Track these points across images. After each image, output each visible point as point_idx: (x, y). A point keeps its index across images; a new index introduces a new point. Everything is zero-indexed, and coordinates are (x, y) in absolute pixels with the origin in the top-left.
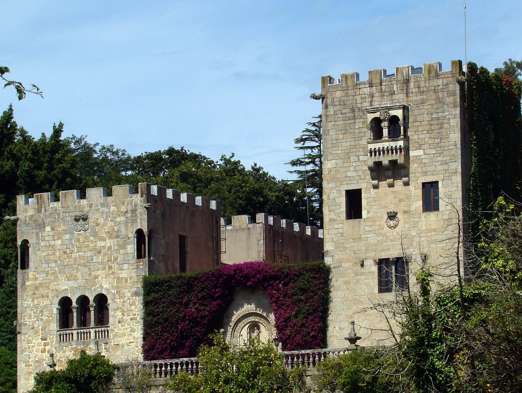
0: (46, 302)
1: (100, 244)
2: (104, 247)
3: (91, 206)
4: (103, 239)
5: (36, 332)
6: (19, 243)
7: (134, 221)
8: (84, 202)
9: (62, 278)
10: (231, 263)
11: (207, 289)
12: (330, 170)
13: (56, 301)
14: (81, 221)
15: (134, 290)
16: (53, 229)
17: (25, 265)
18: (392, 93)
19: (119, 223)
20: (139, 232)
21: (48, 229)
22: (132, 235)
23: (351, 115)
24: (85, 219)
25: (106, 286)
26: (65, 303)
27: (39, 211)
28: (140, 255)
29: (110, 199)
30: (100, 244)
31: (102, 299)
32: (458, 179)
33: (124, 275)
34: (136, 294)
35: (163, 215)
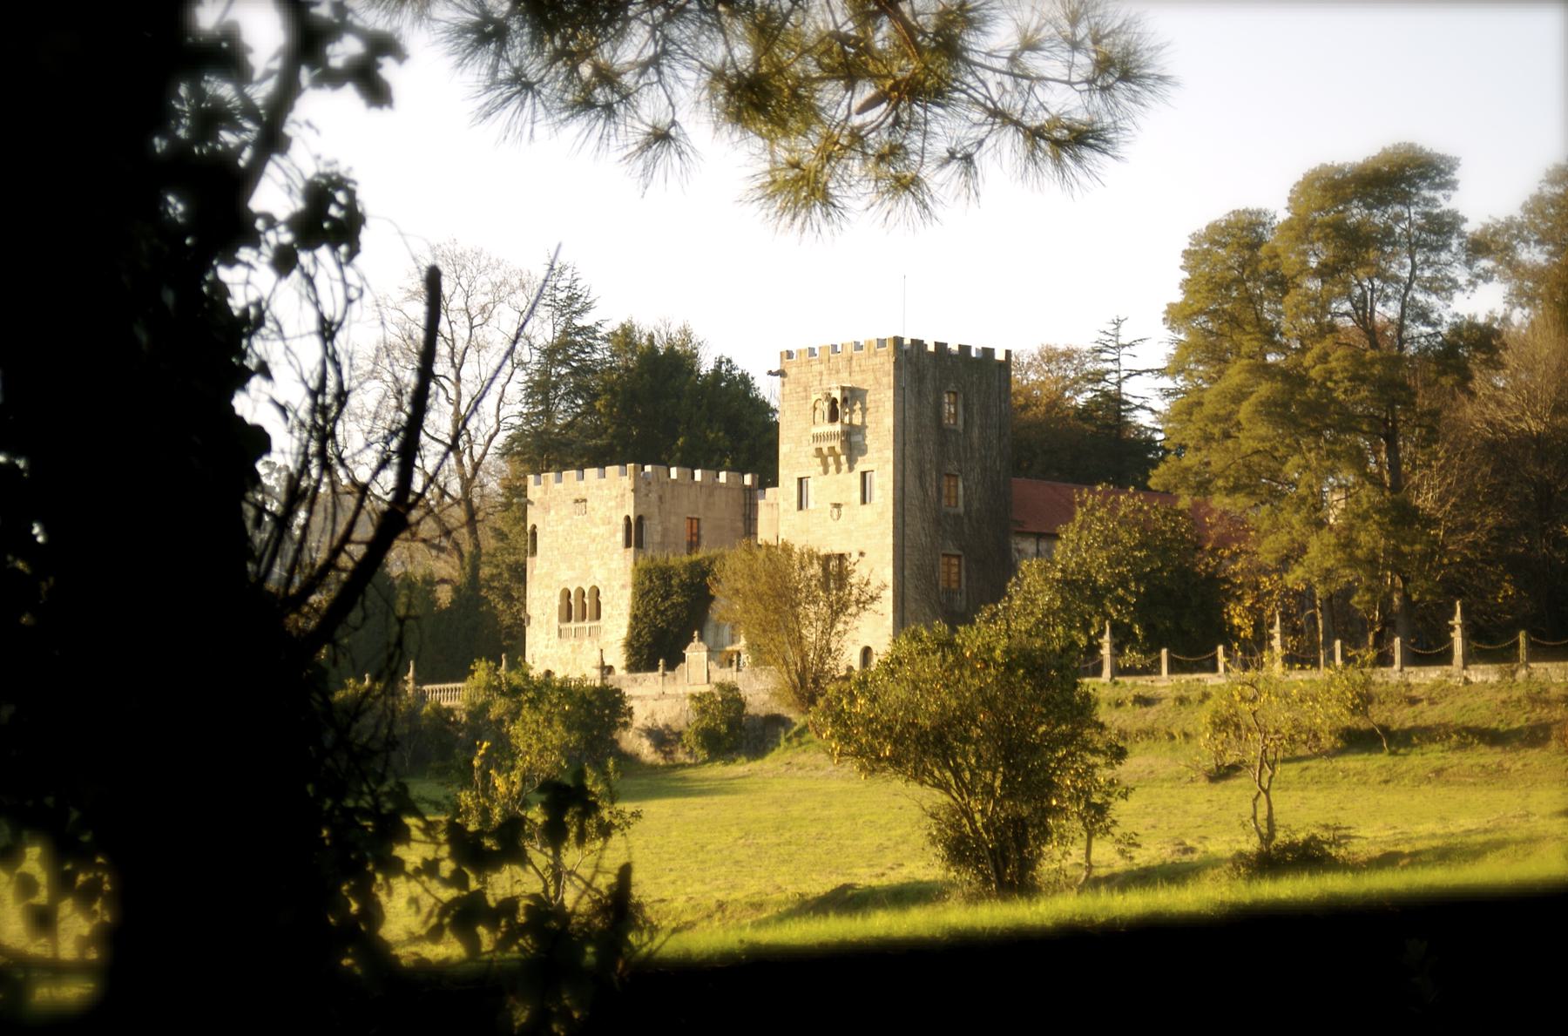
0: (550, 593)
1: (595, 531)
2: (597, 535)
3: (587, 488)
4: (596, 525)
5: (541, 627)
6: (529, 527)
7: (623, 507)
8: (582, 483)
9: (563, 566)
10: (238, 411)
11: (1014, 778)
12: (785, 455)
13: (558, 592)
14: (1196, 410)
15: (621, 582)
16: (557, 513)
17: (534, 552)
18: (838, 372)
19: (611, 508)
20: (628, 518)
21: (552, 512)
22: (621, 522)
23: (803, 394)
24: (585, 500)
25: (598, 577)
26: (567, 594)
27: (546, 493)
28: (628, 545)
29: (603, 480)
30: (595, 531)
31: (596, 592)
32: (890, 468)
33: (614, 565)
34: (624, 587)
35: (660, 498)
